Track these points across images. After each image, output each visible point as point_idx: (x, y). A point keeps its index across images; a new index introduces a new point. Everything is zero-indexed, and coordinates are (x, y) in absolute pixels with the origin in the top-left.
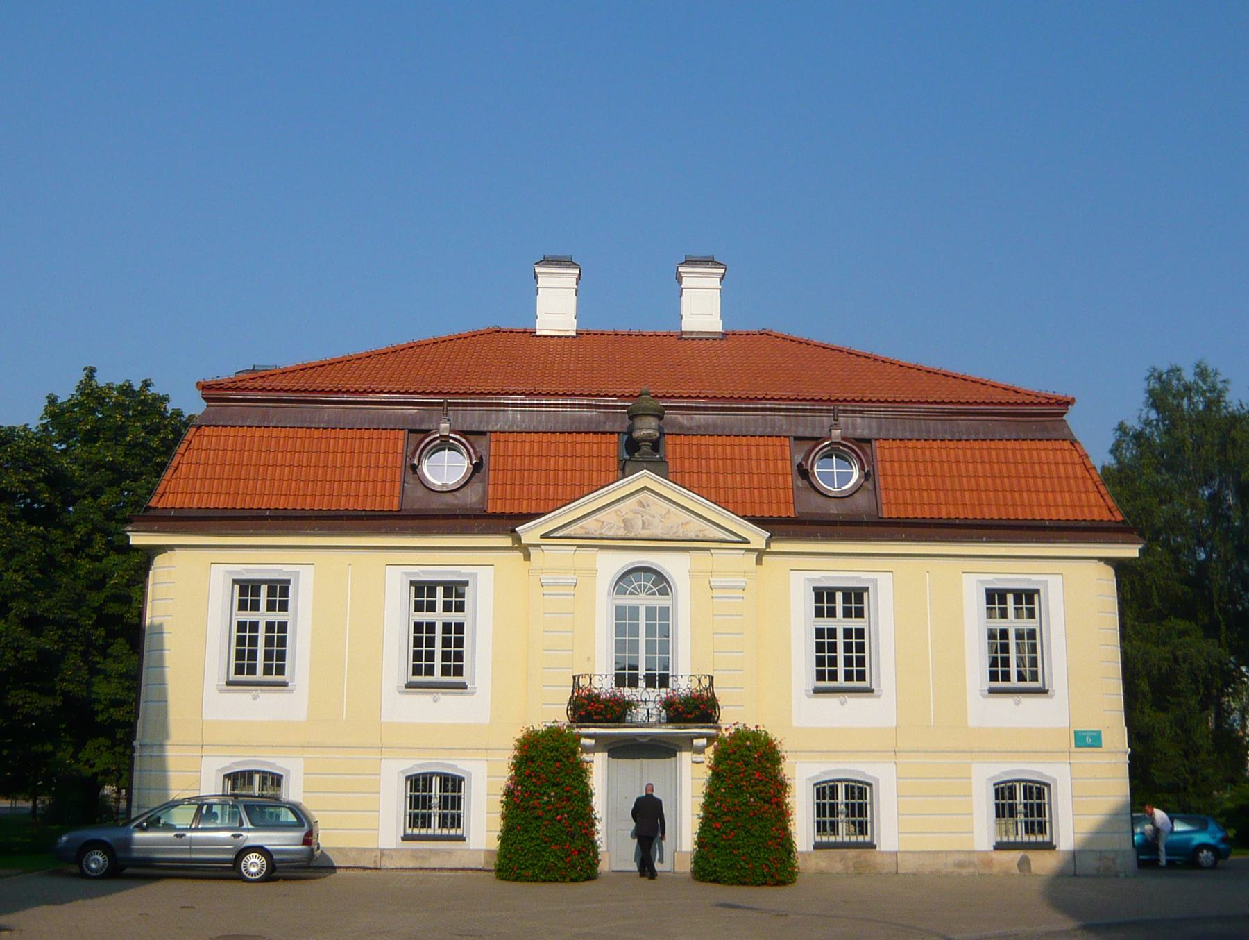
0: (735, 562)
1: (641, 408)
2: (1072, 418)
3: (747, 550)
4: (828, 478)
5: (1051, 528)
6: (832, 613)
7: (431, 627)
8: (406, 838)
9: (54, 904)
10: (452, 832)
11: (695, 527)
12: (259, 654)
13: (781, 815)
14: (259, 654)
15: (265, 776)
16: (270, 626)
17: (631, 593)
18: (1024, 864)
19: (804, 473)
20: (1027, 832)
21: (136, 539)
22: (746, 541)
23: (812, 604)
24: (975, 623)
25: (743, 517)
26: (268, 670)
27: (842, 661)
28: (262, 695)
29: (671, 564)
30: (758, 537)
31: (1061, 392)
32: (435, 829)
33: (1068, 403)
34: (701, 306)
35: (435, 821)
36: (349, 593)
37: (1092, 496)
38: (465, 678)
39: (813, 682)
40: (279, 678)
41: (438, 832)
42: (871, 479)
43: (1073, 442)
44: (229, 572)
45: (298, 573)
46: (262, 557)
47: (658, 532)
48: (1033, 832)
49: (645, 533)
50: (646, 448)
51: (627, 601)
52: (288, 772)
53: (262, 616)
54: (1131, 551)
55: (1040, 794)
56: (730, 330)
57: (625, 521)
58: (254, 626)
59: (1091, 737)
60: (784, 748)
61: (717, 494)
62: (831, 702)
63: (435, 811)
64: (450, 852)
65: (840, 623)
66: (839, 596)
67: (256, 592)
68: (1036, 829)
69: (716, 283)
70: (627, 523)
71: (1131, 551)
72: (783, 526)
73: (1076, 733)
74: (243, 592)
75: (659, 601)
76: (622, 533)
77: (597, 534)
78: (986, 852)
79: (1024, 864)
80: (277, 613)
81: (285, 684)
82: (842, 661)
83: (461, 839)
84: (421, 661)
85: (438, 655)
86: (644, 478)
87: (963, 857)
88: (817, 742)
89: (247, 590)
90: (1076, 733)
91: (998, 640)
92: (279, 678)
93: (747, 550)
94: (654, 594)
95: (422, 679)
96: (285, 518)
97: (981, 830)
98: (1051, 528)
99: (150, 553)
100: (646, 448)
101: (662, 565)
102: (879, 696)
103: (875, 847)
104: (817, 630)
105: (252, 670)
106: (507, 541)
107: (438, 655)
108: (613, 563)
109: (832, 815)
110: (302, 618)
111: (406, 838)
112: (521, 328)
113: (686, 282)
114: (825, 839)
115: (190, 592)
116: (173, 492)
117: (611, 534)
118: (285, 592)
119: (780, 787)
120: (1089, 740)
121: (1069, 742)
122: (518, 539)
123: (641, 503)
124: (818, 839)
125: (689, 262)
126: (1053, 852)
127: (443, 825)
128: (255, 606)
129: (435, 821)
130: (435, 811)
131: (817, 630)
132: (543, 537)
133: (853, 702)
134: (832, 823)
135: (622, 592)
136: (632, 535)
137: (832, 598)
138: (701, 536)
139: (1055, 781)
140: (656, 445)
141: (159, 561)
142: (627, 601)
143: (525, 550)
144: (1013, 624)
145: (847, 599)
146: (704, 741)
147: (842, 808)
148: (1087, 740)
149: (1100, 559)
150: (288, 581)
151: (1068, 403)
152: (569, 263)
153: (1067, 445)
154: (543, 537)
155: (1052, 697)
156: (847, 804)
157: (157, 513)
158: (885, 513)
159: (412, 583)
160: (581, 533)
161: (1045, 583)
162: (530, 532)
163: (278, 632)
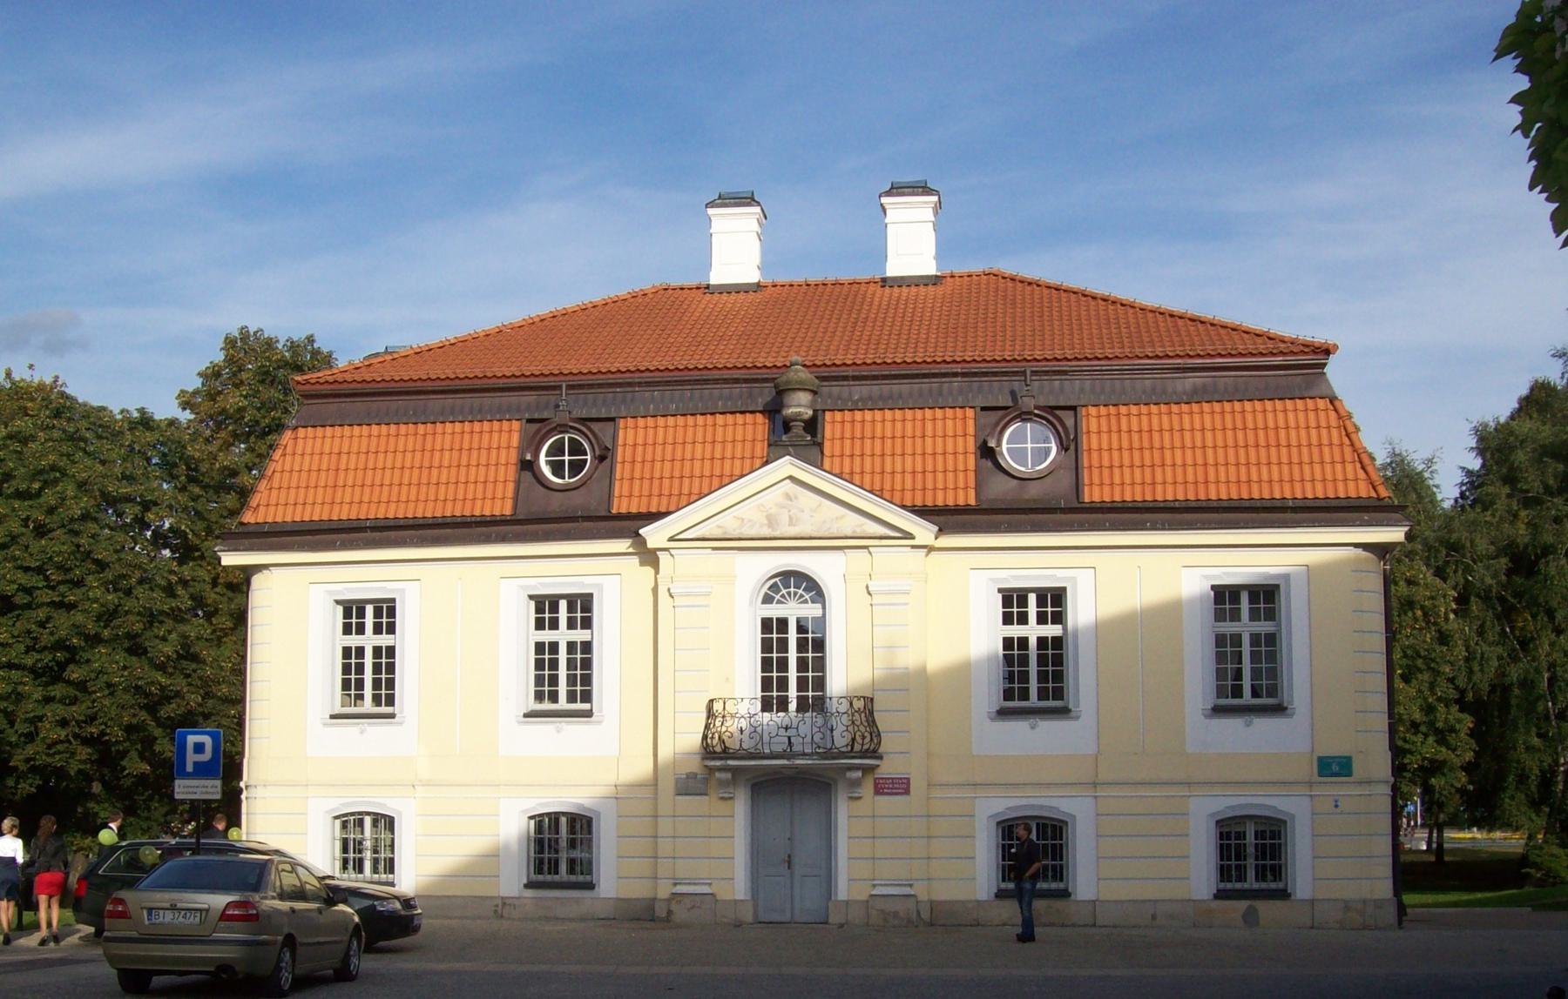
0: (893, 561)
1: (788, 380)
2: (1335, 371)
3: (913, 547)
4: (1019, 455)
5: (1295, 510)
6: (1023, 619)
7: (554, 647)
8: (530, 885)
10: (1054, 885)
11: (852, 523)
12: (369, 681)
14: (369, 681)
15: (377, 818)
16: (377, 651)
17: (779, 602)
18: (1250, 918)
19: (987, 453)
20: (1257, 879)
21: (229, 559)
22: (910, 536)
23: (999, 610)
24: (516, 638)
25: (903, 507)
26: (1043, 694)
28: (565, 726)
30: (924, 531)
31: (1319, 336)
32: (1251, 883)
33: (1327, 351)
34: (911, 243)
35: (1251, 874)
36: (466, 609)
37: (1349, 467)
38: (397, 709)
39: (997, 701)
40: (389, 710)
41: (1256, 886)
42: (607, 462)
43: (1333, 400)
44: (330, 593)
45: (403, 591)
47: (806, 529)
48: (1264, 880)
49: (792, 531)
50: (798, 428)
52: (1293, 817)
53: (1246, 627)
54: (1394, 535)
55: (1276, 835)
56: (768, 281)
57: (769, 517)
58: (554, 647)
59: (1339, 764)
61: (867, 478)
62: (1019, 727)
63: (1251, 862)
64: (577, 901)
65: (369, 640)
66: (1032, 598)
67: (554, 608)
68: (546, 868)
69: (929, 214)
70: (771, 521)
71: (1394, 535)
72: (948, 518)
74: (347, 613)
75: (811, 611)
76: (766, 532)
77: (736, 534)
79: (1250, 918)
81: (392, 716)
83: (590, 886)
84: (545, 686)
85: (564, 678)
86: (786, 466)
89: (352, 611)
90: (1320, 759)
91: (545, 655)
92: (389, 710)
93: (913, 547)
94: (806, 602)
95: (1016, 704)
96: (1283, 509)
97: (1198, 874)
98: (1295, 510)
99: (248, 572)
100: (798, 428)
102: (600, 722)
103: (1069, 895)
104: (1005, 639)
106: (623, 545)
107: (564, 678)
109: (1238, 858)
110: (411, 642)
111: (530, 885)
112: (694, 282)
113: (891, 215)
114: (1229, 886)
115: (292, 613)
116: (266, 507)
117: (752, 533)
118: (392, 612)
120: (1335, 768)
121: (1309, 770)
122: (640, 542)
123: (788, 496)
124: (1222, 886)
125: (896, 190)
126: (1288, 903)
127: (1261, 876)
128: (554, 625)
129: (1251, 874)
130: (1251, 862)
131: (1005, 639)
132: (671, 539)
133: (1047, 726)
134: (1238, 867)
135: (767, 600)
136: (777, 534)
137: (1023, 602)
138: (859, 533)
140: (812, 426)
141: (257, 581)
142: (775, 611)
143: (649, 557)
145: (1041, 602)
146: (859, 774)
147: (1251, 850)
148: (1334, 767)
149: (1356, 545)
150: (393, 600)
151: (1327, 351)
152: (925, 190)
153: (1321, 403)
154: (671, 539)
155: (1291, 715)
157: (251, 529)
158: (1092, 494)
159: (531, 597)
160: (718, 533)
161: (600, 587)
162: (655, 534)
163: (1268, 647)
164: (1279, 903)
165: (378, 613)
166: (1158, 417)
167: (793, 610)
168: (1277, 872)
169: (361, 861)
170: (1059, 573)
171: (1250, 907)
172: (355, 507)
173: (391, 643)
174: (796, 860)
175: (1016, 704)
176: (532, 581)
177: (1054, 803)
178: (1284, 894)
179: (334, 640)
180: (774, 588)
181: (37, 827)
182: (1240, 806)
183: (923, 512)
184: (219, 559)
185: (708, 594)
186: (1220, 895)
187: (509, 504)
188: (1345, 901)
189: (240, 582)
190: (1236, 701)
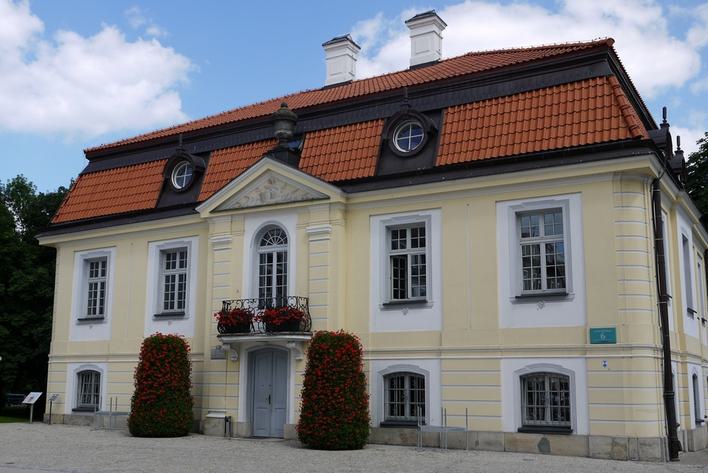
0: (320, 218)
9: (351, 448)
13: (362, 401)
16: (415, 257)
22: (329, 198)
27: (407, 282)
29: (289, 223)
30: (336, 195)
32: (548, 421)
45: (430, 216)
46: (536, 188)
49: (273, 201)
51: (266, 250)
57: (261, 195)
60: (366, 345)
70: (262, 196)
73: (591, 330)
76: (259, 203)
78: (512, 433)
80: (399, 250)
82: (407, 282)
87: (492, 437)
88: (387, 339)
90: (591, 330)
101: (284, 223)
105: (538, 285)
108: (253, 226)
114: (532, 422)
118: (423, 231)
119: (359, 380)
121: (581, 340)
135: (263, 243)
139: (428, 373)
142: (266, 250)
144: (409, 251)
147: (407, 393)
148: (603, 337)
149: (615, 174)
154: (212, 212)
155: (572, 299)
156: (407, 389)
164: (564, 437)
165: (414, 234)
166: (490, 108)
167: (274, 249)
168: (567, 416)
169: (403, 406)
170: (421, 214)
171: (543, 439)
172: (598, 135)
173: (422, 252)
174: (273, 398)
175: (92, 316)
176: (519, 203)
177: (416, 363)
178: (567, 431)
179: (430, 251)
180: (266, 236)
181: (143, 376)
182: (393, 367)
183: (335, 184)
184: (38, 242)
185: (228, 242)
186: (524, 430)
187: (373, 170)
188: (613, 439)
189: (49, 256)
190: (538, 292)
